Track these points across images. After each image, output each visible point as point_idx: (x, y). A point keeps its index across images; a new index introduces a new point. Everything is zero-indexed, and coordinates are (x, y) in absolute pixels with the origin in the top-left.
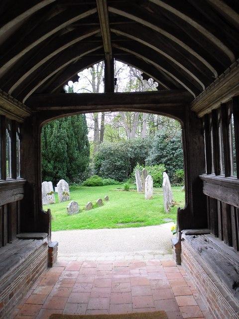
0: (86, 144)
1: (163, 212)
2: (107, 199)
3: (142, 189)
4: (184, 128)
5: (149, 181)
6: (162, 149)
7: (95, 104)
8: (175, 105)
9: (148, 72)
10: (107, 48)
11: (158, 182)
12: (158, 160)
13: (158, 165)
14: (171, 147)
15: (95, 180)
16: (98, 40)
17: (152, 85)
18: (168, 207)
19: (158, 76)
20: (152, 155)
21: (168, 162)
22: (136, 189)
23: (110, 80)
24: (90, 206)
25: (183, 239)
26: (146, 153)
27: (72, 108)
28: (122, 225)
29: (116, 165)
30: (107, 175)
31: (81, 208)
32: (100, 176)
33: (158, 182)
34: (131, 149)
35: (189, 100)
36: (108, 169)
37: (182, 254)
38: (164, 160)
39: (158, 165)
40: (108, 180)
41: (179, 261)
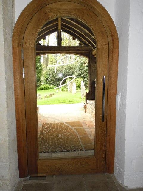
0: (41, 66)
1: (81, 98)
2: (54, 94)
3: (71, 89)
4: (89, 61)
5: (75, 86)
6: (81, 70)
7: (54, 50)
8: (86, 52)
9: (75, 37)
10: (59, 28)
11: (79, 87)
12: (79, 76)
13: (79, 78)
14: (86, 69)
15: (45, 86)
16: (57, 25)
17: (76, 43)
18: (83, 97)
19: (79, 39)
20: (77, 72)
21: (85, 77)
22: (67, 90)
23: (59, 39)
24: (46, 97)
25: (87, 103)
26: (73, 72)
27: (45, 52)
28: (62, 103)
29: (56, 78)
30: (52, 83)
31: (42, 97)
32: (48, 84)
33: (79, 87)
34: (65, 70)
35: (91, 51)
36: (52, 80)
37: (87, 109)
38: (82, 76)
39: (79, 78)
40: (52, 86)
41: (86, 111)
